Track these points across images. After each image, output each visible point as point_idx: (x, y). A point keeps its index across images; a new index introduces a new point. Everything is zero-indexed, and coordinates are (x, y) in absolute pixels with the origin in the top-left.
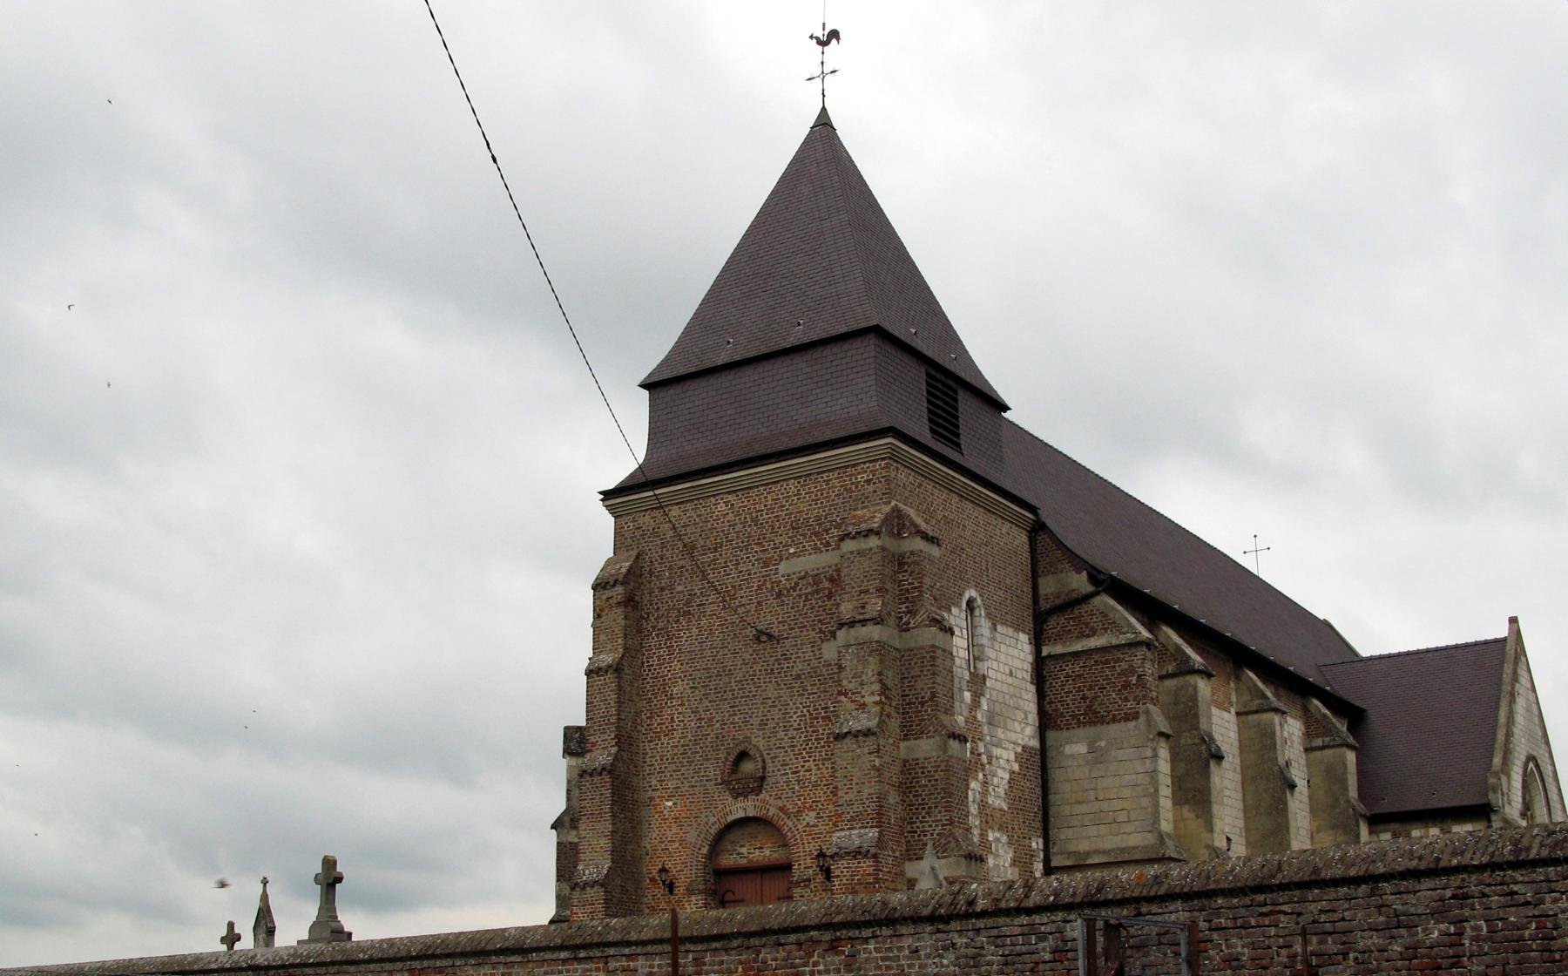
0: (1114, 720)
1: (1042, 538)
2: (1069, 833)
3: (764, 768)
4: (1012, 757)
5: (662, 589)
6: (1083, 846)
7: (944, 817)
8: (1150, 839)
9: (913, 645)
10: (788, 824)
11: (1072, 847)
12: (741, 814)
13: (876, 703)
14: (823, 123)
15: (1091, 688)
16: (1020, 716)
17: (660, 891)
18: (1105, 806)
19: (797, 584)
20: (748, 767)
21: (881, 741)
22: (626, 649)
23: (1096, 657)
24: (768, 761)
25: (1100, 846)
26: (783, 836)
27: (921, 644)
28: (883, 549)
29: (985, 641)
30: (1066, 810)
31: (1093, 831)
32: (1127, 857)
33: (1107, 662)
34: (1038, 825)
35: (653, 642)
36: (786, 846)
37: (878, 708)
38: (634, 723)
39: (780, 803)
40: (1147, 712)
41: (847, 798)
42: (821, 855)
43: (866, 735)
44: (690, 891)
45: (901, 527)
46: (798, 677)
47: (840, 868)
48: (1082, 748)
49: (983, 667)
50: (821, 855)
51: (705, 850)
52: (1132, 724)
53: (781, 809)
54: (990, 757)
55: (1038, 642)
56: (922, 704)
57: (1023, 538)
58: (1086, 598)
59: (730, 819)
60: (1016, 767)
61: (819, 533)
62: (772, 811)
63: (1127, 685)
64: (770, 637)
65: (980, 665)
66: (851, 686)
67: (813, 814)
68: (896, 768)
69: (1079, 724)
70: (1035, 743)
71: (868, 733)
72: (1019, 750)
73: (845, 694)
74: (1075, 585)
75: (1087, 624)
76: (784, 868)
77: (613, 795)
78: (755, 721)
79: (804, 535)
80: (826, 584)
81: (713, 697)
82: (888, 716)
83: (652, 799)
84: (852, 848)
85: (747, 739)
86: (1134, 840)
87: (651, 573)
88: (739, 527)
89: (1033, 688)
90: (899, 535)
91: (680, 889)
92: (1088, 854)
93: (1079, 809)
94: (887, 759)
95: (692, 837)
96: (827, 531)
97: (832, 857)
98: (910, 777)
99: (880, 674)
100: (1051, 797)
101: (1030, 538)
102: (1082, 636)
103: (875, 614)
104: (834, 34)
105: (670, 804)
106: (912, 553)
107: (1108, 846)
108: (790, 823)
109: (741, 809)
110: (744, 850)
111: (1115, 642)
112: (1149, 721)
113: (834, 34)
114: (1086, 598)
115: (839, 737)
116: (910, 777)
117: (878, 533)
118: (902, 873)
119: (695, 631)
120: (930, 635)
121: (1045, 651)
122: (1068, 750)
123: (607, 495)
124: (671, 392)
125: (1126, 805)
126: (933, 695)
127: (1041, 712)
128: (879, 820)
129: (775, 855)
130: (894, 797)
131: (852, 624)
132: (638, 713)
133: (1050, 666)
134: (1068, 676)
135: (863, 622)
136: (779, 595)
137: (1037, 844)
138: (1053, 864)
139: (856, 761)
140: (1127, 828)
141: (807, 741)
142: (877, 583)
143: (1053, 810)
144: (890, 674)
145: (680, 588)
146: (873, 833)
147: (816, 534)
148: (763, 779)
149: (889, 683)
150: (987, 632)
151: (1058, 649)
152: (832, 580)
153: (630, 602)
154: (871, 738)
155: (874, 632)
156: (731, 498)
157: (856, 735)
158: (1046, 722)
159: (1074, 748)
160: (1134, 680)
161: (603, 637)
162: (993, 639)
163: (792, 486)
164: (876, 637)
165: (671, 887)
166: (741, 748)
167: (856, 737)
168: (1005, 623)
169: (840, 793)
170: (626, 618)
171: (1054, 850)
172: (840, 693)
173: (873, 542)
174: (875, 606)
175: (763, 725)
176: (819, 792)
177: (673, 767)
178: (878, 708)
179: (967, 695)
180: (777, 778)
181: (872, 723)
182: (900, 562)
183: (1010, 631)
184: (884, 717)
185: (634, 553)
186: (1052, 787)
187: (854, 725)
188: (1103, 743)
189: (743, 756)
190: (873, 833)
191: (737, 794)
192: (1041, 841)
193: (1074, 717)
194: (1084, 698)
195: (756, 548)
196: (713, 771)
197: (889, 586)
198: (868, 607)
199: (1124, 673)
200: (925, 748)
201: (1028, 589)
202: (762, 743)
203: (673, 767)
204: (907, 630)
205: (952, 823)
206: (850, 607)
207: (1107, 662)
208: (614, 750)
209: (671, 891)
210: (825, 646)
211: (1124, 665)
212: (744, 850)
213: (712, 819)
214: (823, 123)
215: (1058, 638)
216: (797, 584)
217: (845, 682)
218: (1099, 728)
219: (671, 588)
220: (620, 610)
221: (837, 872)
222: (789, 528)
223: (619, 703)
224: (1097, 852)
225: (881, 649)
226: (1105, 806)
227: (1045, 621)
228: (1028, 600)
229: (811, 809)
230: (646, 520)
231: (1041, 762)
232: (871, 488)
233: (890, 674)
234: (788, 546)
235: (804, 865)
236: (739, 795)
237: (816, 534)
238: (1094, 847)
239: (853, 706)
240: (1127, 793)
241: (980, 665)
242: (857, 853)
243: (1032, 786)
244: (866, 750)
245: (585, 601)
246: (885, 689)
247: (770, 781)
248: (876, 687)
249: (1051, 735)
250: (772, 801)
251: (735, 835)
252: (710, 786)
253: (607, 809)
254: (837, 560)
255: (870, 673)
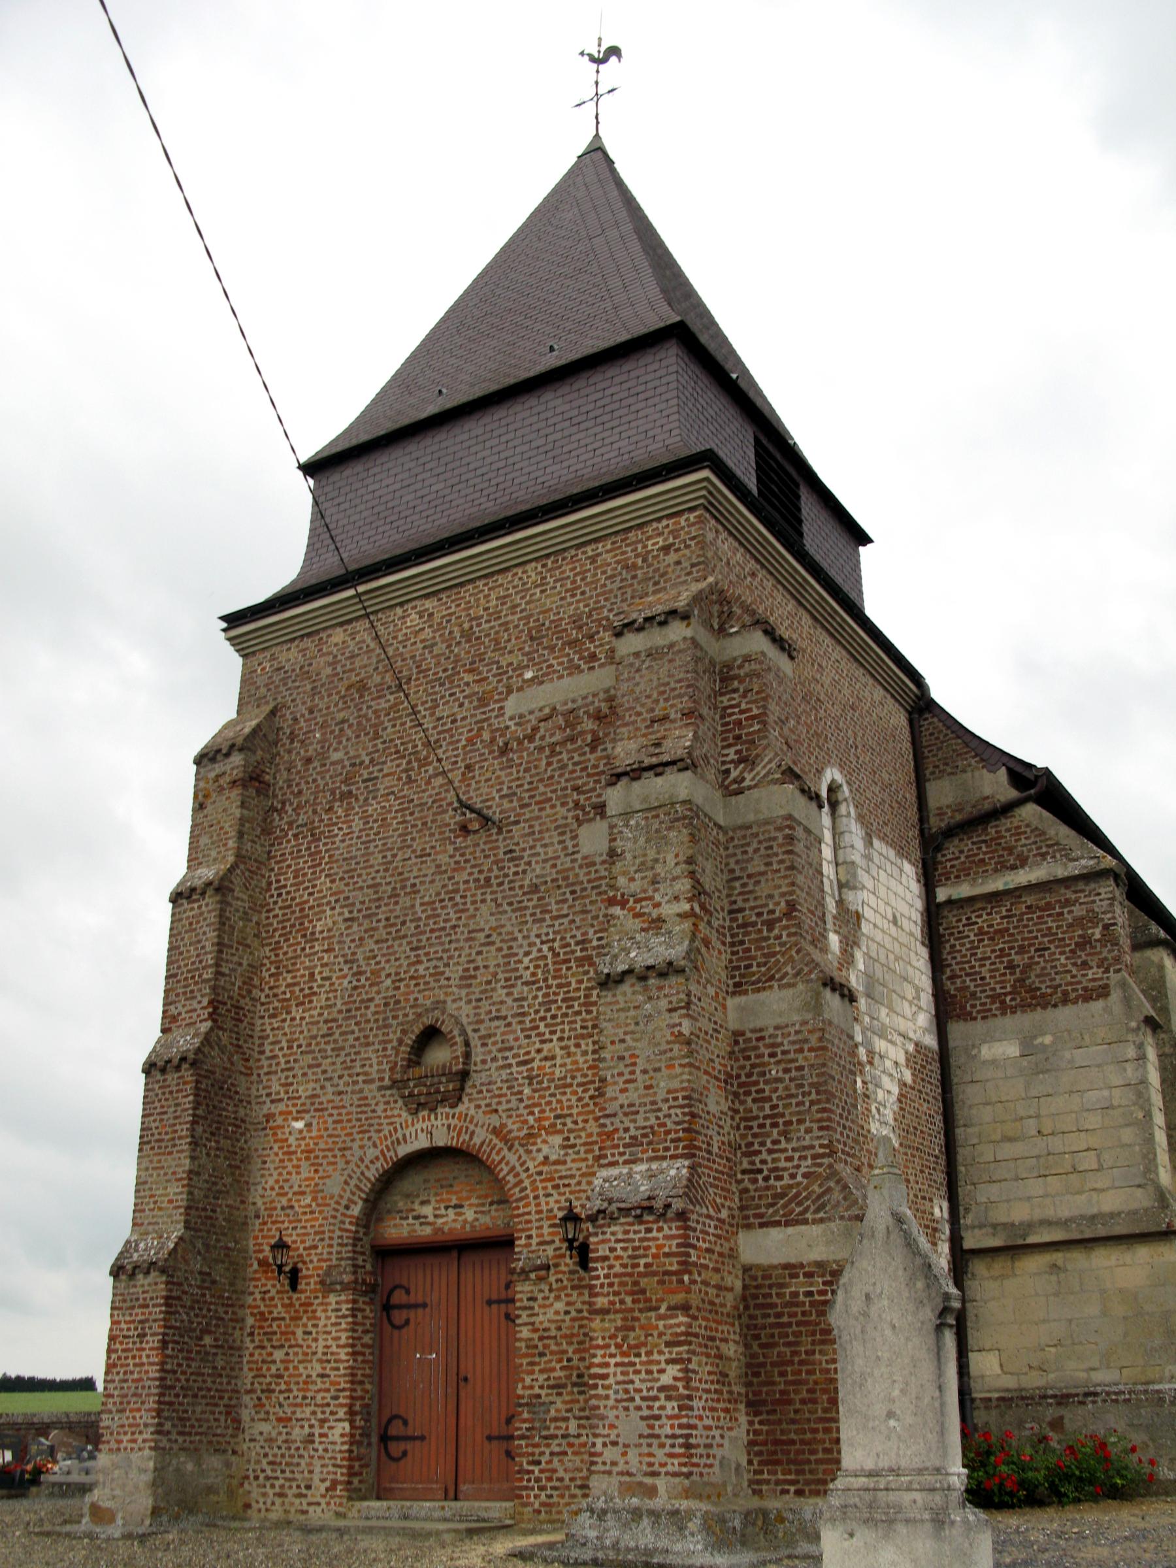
0: (1065, 1001)
1: (929, 723)
2: (993, 1191)
3: (467, 1055)
4: (902, 1059)
5: (309, 761)
6: (1019, 1213)
7: (814, 1139)
8: (1142, 1199)
9: (751, 817)
10: (507, 1160)
11: (1000, 1215)
12: (423, 1143)
13: (683, 916)
14: (596, 153)
15: (1022, 950)
16: (910, 993)
17: (274, 1286)
18: (1056, 1144)
19: (535, 729)
20: (439, 1056)
21: (693, 988)
22: (238, 856)
23: (1029, 900)
24: (475, 1042)
25: (1050, 1213)
26: (499, 1183)
27: (765, 814)
28: (694, 642)
29: (856, 857)
30: (987, 1153)
31: (1035, 1187)
32: (1101, 1231)
33: (1049, 907)
34: (940, 1177)
35: (288, 847)
36: (503, 1201)
37: (687, 925)
38: (248, 982)
39: (495, 1121)
40: (1123, 985)
41: (623, 1099)
42: (571, 1217)
43: (662, 975)
44: (327, 1287)
45: (726, 617)
46: (535, 888)
47: (607, 1241)
48: (1012, 1049)
49: (854, 899)
50: (571, 1217)
51: (356, 1210)
52: (1097, 1006)
53: (496, 1131)
54: (871, 1053)
55: (929, 879)
56: (770, 925)
57: (899, 719)
58: (1008, 809)
59: (403, 1150)
60: (908, 1077)
61: (579, 644)
62: (481, 1135)
63: (1085, 942)
64: (486, 820)
65: (850, 896)
66: (635, 887)
67: (557, 1140)
68: (720, 1046)
69: (1004, 1009)
70: (931, 1041)
71: (667, 970)
72: (911, 1048)
73: (623, 904)
74: (987, 791)
75: (1010, 850)
76: (503, 1243)
77: (197, 1105)
78: (454, 972)
79: (552, 649)
80: (589, 725)
81: (382, 933)
82: (707, 943)
83: (269, 1117)
84: (634, 1200)
85: (439, 1005)
86: (1110, 1202)
87: (292, 737)
88: (441, 648)
89: (924, 952)
90: (722, 632)
91: (309, 1283)
92: (1029, 1226)
93: (1008, 1150)
94: (704, 1024)
95: (334, 1186)
96: (591, 638)
97: (592, 1219)
98: (746, 1065)
99: (690, 861)
100: (960, 1132)
101: (911, 722)
102: (1003, 867)
103: (680, 753)
104: (614, 51)
105: (299, 1125)
106: (747, 659)
107: (1064, 1213)
108: (512, 1158)
109: (422, 1132)
110: (427, 1210)
111: (1061, 872)
112: (1127, 1000)
113: (614, 51)
114: (1008, 809)
115: (608, 982)
116: (746, 1065)
117: (685, 617)
118: (733, 1254)
119: (357, 824)
120: (782, 800)
121: (942, 895)
122: (986, 1052)
123: (233, 620)
124: (348, 472)
125: (1093, 1141)
126: (792, 906)
127: (939, 994)
128: (690, 1144)
129: (485, 1220)
130: (716, 1102)
131: (635, 773)
132: (255, 968)
133: (950, 917)
134: (981, 932)
135: (658, 769)
136: (505, 750)
137: (940, 1210)
138: (968, 1244)
139: (643, 1028)
140: (1101, 1181)
141: (547, 1004)
142: (685, 703)
143: (963, 1153)
144: (709, 866)
145: (336, 756)
146: (677, 1170)
147: (573, 643)
148: (464, 1075)
149: (708, 883)
150: (859, 844)
151: (965, 890)
152: (598, 717)
153: (254, 781)
154: (673, 980)
155: (679, 785)
156: (429, 604)
157: (643, 975)
158: (947, 1008)
159: (996, 1047)
160: (1097, 933)
161: (204, 840)
162: (868, 858)
163: (532, 572)
164: (683, 794)
165: (294, 1278)
166: (427, 1021)
167: (643, 978)
168: (883, 838)
169: (610, 1092)
170: (243, 805)
171: (967, 1220)
172: (612, 902)
173: (677, 631)
174: (679, 740)
175: (467, 978)
176: (569, 1098)
177: (308, 1059)
178: (687, 925)
179: (834, 940)
180: (488, 1074)
181: (676, 952)
182: (725, 676)
183: (891, 853)
184: (698, 945)
185: (267, 709)
186: (961, 1114)
187: (639, 958)
188: (1048, 1040)
189: (430, 1035)
190: (677, 1170)
191: (419, 1105)
192: (945, 1205)
193: (994, 998)
194: (1011, 967)
195: (468, 678)
196: (378, 1063)
197: (705, 711)
198: (668, 744)
199: (1079, 922)
200: (777, 1007)
201: (911, 795)
202: (465, 1012)
203: (308, 1059)
204: (740, 792)
205: (832, 1153)
206: (632, 746)
207: (1049, 907)
208: (205, 1027)
209: (294, 1285)
210: (584, 831)
211: (1078, 911)
212: (427, 1210)
213: (371, 1153)
214: (596, 153)
215: (963, 873)
216: (535, 729)
217: (622, 881)
218: (1038, 1015)
219: (323, 756)
220: (235, 794)
221: (603, 1251)
222: (530, 647)
223: (220, 946)
224: (1048, 1223)
225: (691, 816)
226: (1056, 1144)
227: (938, 849)
228: (912, 814)
229: (552, 1130)
230: (291, 656)
231: (942, 1070)
232: (672, 557)
233: (709, 866)
234: (523, 667)
235: (538, 1240)
236: (421, 1106)
237: (573, 643)
238: (1038, 1214)
239: (638, 924)
240: (1093, 1121)
241: (850, 896)
242: (645, 1211)
243: (931, 1108)
244: (663, 1004)
245: (183, 780)
246: (698, 892)
247: (477, 1079)
248: (684, 885)
249: (957, 1030)
250: (480, 1117)
251: (412, 1182)
252: (371, 1090)
253: (183, 1129)
254: (609, 682)
255: (671, 861)
